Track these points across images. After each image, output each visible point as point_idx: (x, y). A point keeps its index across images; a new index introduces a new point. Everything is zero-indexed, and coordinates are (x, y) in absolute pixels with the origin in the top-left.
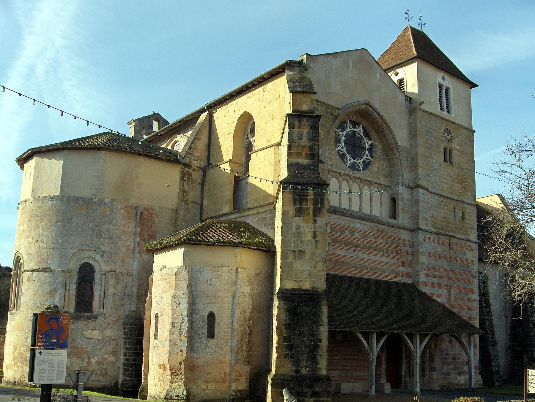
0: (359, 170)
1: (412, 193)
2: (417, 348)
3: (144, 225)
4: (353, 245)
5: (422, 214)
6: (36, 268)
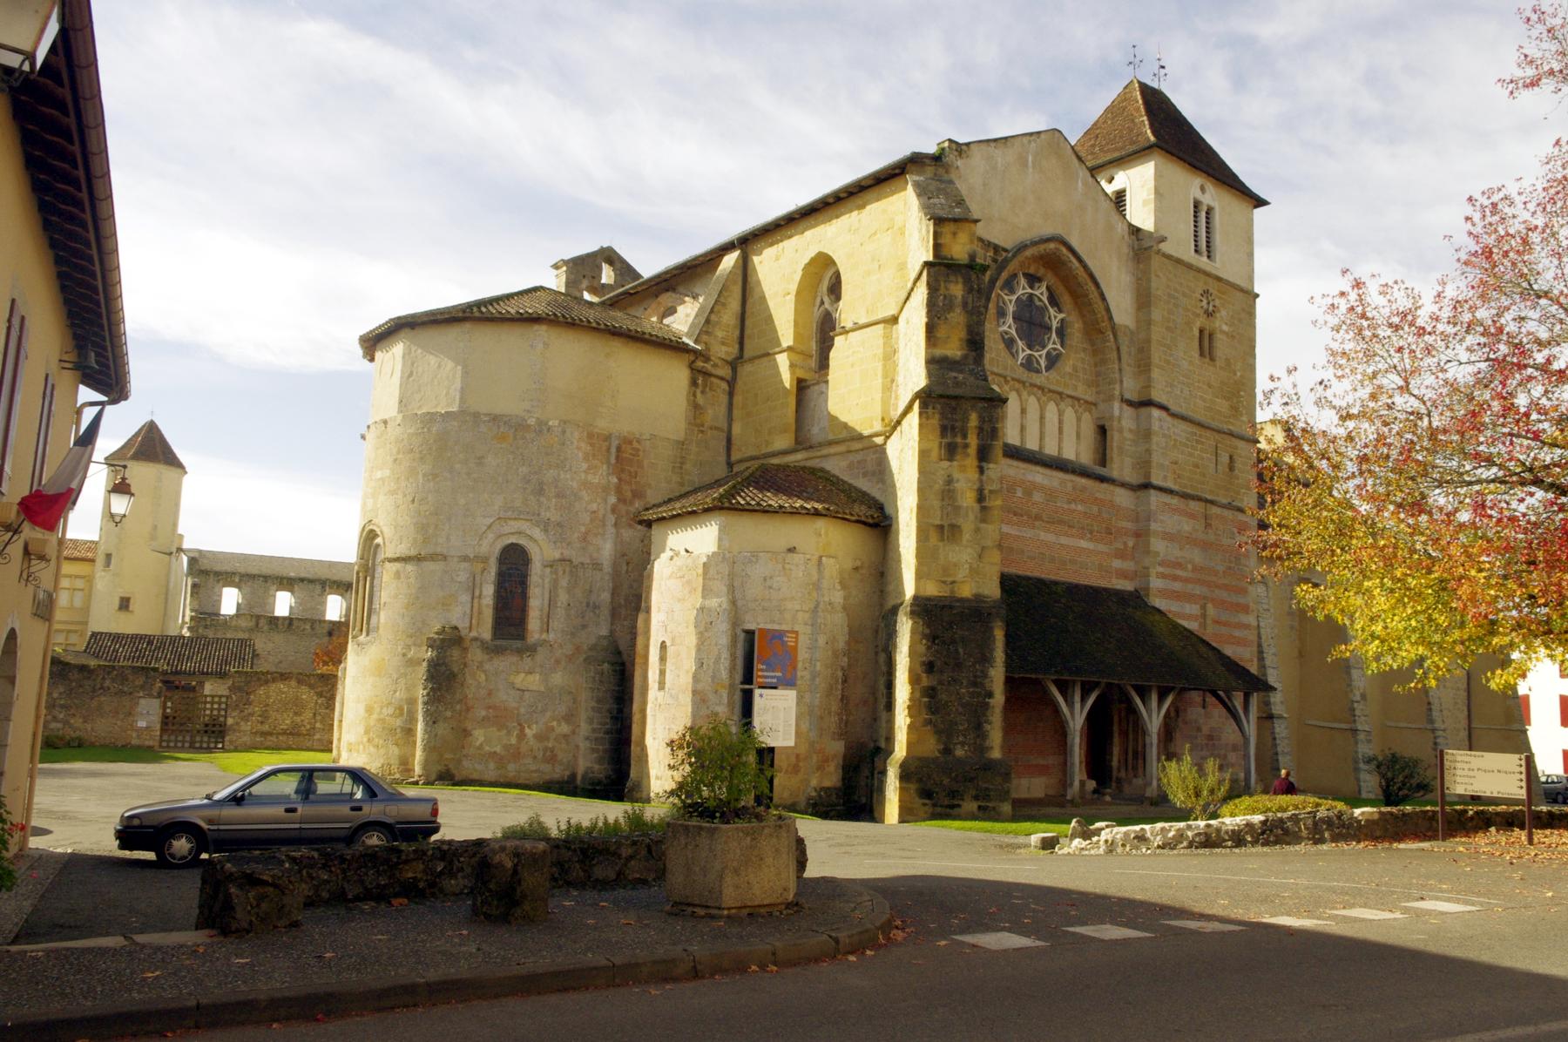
0: (1038, 371)
1: (1138, 417)
2: (1153, 717)
3: (623, 470)
4: (1029, 517)
5: (1156, 458)
6: (413, 552)
